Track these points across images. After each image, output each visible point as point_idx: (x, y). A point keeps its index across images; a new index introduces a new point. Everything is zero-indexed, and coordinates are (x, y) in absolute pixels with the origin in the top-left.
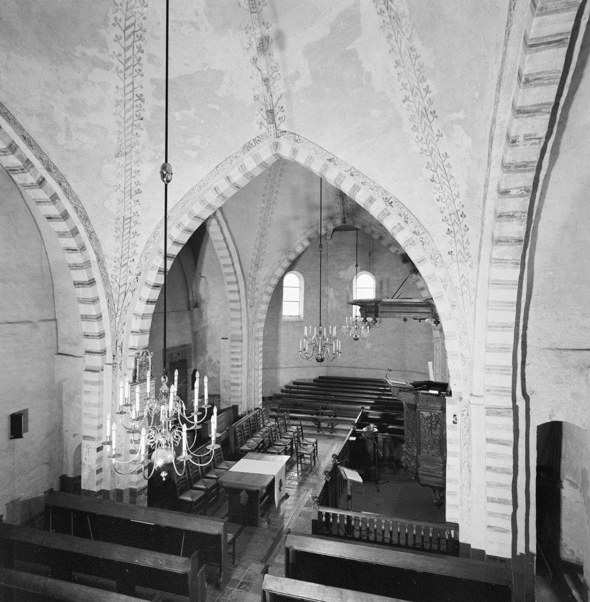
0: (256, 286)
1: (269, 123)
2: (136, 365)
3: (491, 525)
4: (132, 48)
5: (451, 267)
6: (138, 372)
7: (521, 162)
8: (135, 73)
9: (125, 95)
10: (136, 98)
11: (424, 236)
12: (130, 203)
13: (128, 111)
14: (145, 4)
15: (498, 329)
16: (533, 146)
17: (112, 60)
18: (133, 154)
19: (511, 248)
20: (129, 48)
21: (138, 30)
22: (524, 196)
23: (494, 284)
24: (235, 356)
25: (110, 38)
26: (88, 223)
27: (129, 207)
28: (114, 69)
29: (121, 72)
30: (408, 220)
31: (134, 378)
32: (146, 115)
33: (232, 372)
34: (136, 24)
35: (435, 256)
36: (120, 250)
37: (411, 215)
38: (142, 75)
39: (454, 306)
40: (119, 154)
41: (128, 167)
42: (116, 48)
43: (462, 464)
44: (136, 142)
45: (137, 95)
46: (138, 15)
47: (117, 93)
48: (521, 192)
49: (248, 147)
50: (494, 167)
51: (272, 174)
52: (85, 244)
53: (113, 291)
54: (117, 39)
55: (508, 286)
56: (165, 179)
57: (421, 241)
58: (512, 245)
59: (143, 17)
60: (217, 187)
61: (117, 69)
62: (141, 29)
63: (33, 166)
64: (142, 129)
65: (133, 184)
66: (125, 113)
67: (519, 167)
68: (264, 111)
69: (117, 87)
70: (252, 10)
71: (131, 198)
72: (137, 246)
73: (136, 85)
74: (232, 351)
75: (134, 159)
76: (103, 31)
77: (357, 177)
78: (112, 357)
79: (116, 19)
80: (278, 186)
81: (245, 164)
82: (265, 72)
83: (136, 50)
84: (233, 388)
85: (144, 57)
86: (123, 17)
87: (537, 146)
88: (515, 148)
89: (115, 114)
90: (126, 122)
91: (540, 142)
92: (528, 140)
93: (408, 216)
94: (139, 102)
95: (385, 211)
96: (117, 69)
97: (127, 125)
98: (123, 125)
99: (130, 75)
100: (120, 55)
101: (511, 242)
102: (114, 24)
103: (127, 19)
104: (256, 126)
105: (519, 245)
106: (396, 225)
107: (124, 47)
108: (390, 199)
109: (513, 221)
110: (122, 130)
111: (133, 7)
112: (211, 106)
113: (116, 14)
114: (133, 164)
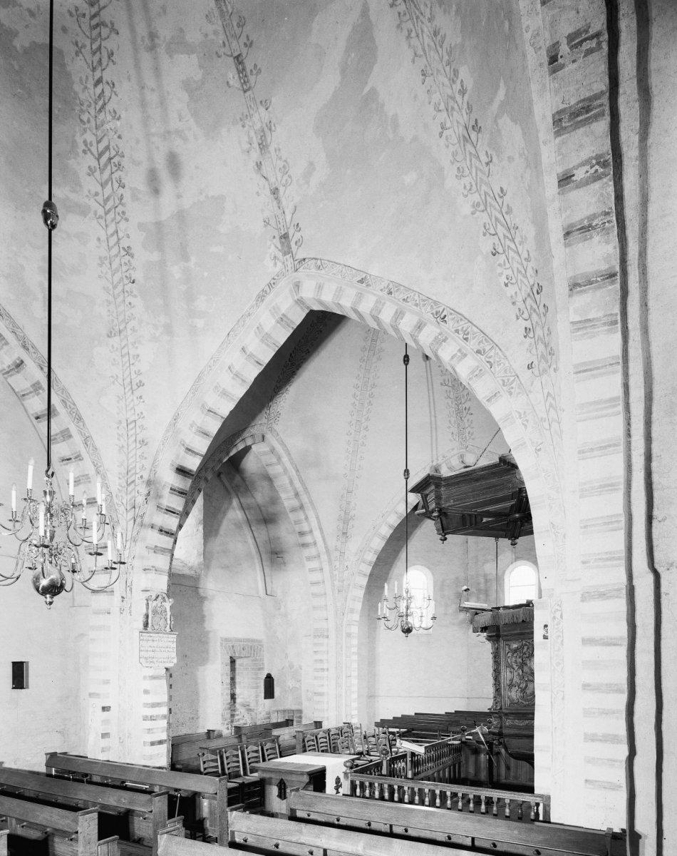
0: (346, 564)
1: (285, 254)
2: (148, 609)
3: (589, 778)
4: (110, 182)
5: (532, 390)
6: (150, 617)
7: (578, 103)
8: (118, 218)
9: (110, 249)
10: (123, 253)
11: (492, 353)
12: (133, 400)
13: (116, 271)
14: (118, 116)
15: (596, 453)
16: (590, 58)
17: (87, 201)
18: (129, 332)
19: (598, 293)
20: (106, 183)
21: (114, 156)
22: (599, 178)
23: (580, 372)
24: (318, 657)
25: (83, 172)
26: (81, 424)
27: (131, 405)
28: (91, 215)
29: (100, 217)
30: (469, 336)
31: (146, 625)
32: (137, 275)
33: (316, 678)
34: (111, 147)
35: (508, 380)
36: (125, 464)
37: (474, 327)
38: (127, 220)
39: (539, 450)
40: (111, 332)
41: (125, 351)
42: (90, 184)
43: (554, 696)
44: (130, 315)
45: (124, 248)
46: (111, 133)
47: (98, 247)
48: (593, 171)
49: (261, 297)
50: (545, 143)
51: (357, 403)
52: (82, 454)
53: (119, 516)
54: (91, 171)
55: (602, 371)
56: (49, 222)
57: (488, 362)
58: (600, 287)
59: (117, 134)
60: (232, 365)
61: (96, 214)
62: (117, 152)
63: (7, 343)
64: (135, 296)
65: (133, 372)
66: (113, 275)
67: (578, 116)
68: (277, 237)
69: (99, 239)
70: (245, 87)
71: (132, 392)
72: (146, 458)
73: (121, 234)
74: (315, 650)
75: (131, 339)
76: (72, 162)
77: (397, 294)
78: (120, 599)
79: (85, 142)
80: (368, 419)
81: (262, 323)
82: (272, 180)
83: (116, 185)
84: (317, 698)
85: (127, 193)
86: (93, 139)
87: (596, 56)
88: (560, 73)
89: (100, 277)
90: (115, 287)
91: (599, 44)
92: (576, 46)
93: (469, 330)
94: (127, 257)
95: (439, 337)
96: (96, 214)
97: (117, 291)
98: (111, 292)
99: (112, 221)
100: (97, 194)
101: (597, 281)
102: (84, 152)
103: (99, 142)
104: (269, 264)
105: (613, 283)
106: (456, 352)
107: (100, 181)
108: (443, 312)
109: (591, 237)
110: (111, 298)
111: (103, 123)
112: (214, 249)
113: (85, 136)
114: (130, 346)
